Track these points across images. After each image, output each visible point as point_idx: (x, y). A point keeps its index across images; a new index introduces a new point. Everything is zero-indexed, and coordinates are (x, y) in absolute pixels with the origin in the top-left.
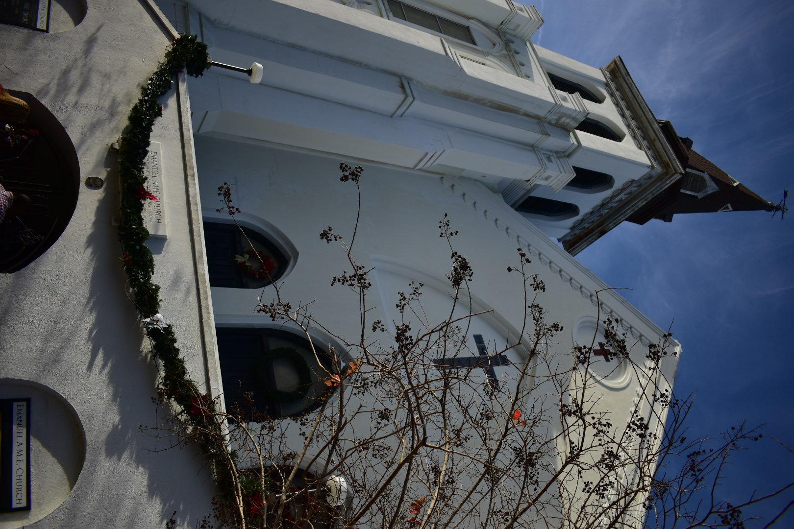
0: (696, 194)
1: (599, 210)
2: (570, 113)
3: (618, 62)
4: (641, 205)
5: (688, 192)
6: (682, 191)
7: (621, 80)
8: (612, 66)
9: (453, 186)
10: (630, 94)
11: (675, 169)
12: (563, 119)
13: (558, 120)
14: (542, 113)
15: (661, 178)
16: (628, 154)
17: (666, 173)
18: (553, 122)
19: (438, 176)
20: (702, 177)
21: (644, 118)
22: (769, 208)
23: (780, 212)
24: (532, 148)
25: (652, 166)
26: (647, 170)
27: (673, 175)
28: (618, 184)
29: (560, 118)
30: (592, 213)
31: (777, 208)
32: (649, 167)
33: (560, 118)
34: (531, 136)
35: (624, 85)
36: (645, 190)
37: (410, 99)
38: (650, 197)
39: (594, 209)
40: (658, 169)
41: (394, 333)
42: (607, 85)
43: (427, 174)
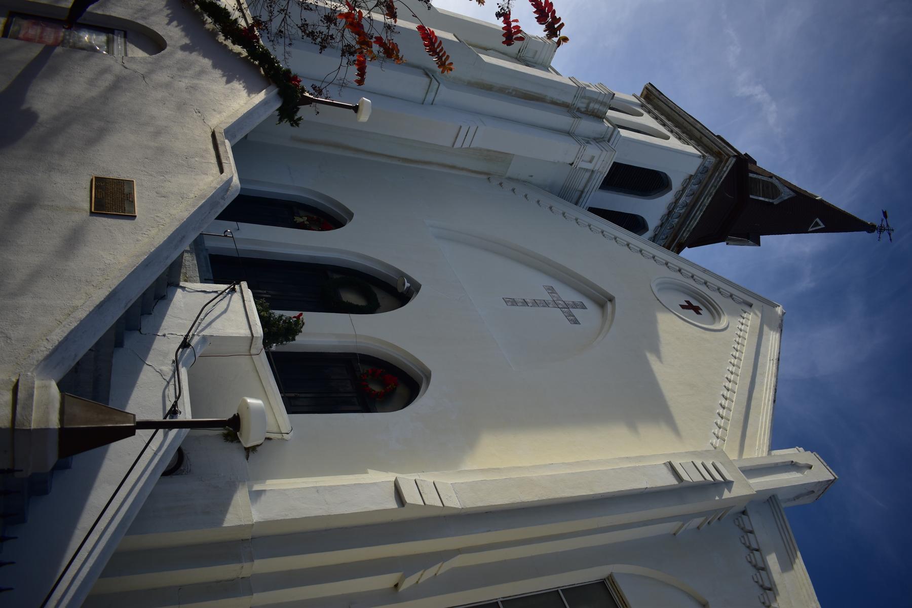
0: (771, 201)
1: (667, 219)
2: (596, 97)
3: (650, 88)
4: (707, 202)
5: (761, 199)
6: (751, 196)
7: (656, 100)
8: (645, 93)
9: (501, 184)
10: (664, 106)
11: (727, 155)
12: (592, 105)
13: (587, 108)
14: (568, 100)
15: (716, 167)
16: (677, 155)
17: (721, 161)
18: (583, 110)
19: (485, 177)
20: (772, 183)
21: (686, 124)
22: (870, 228)
23: (885, 234)
24: (569, 133)
25: (704, 156)
26: (700, 161)
27: (727, 160)
28: (677, 183)
29: (588, 104)
30: (661, 226)
31: (881, 229)
32: (700, 157)
33: (588, 104)
34: (563, 120)
35: (660, 103)
36: (706, 186)
37: (434, 82)
38: (714, 192)
39: (662, 219)
40: (711, 159)
41: (300, 33)
42: (642, 106)
43: (474, 175)
